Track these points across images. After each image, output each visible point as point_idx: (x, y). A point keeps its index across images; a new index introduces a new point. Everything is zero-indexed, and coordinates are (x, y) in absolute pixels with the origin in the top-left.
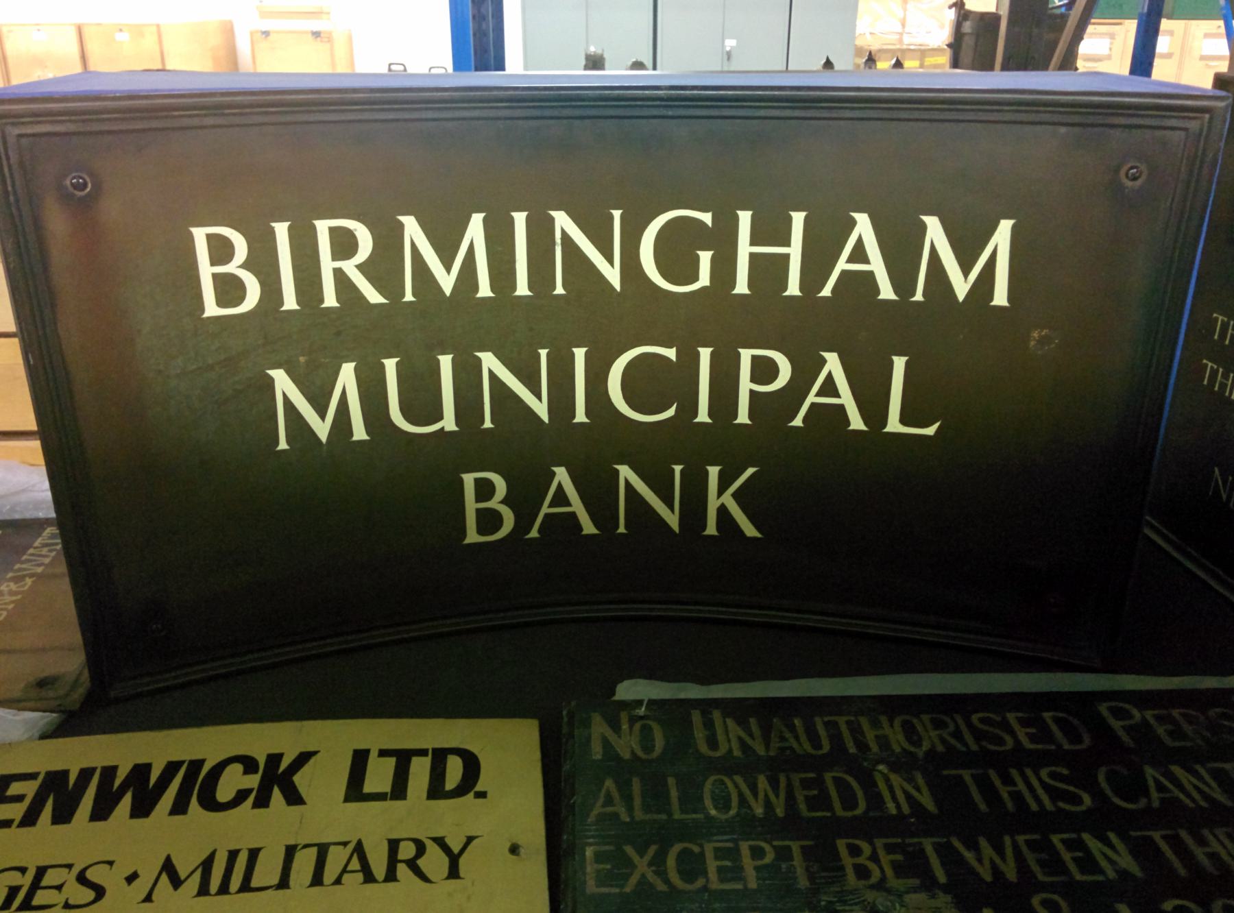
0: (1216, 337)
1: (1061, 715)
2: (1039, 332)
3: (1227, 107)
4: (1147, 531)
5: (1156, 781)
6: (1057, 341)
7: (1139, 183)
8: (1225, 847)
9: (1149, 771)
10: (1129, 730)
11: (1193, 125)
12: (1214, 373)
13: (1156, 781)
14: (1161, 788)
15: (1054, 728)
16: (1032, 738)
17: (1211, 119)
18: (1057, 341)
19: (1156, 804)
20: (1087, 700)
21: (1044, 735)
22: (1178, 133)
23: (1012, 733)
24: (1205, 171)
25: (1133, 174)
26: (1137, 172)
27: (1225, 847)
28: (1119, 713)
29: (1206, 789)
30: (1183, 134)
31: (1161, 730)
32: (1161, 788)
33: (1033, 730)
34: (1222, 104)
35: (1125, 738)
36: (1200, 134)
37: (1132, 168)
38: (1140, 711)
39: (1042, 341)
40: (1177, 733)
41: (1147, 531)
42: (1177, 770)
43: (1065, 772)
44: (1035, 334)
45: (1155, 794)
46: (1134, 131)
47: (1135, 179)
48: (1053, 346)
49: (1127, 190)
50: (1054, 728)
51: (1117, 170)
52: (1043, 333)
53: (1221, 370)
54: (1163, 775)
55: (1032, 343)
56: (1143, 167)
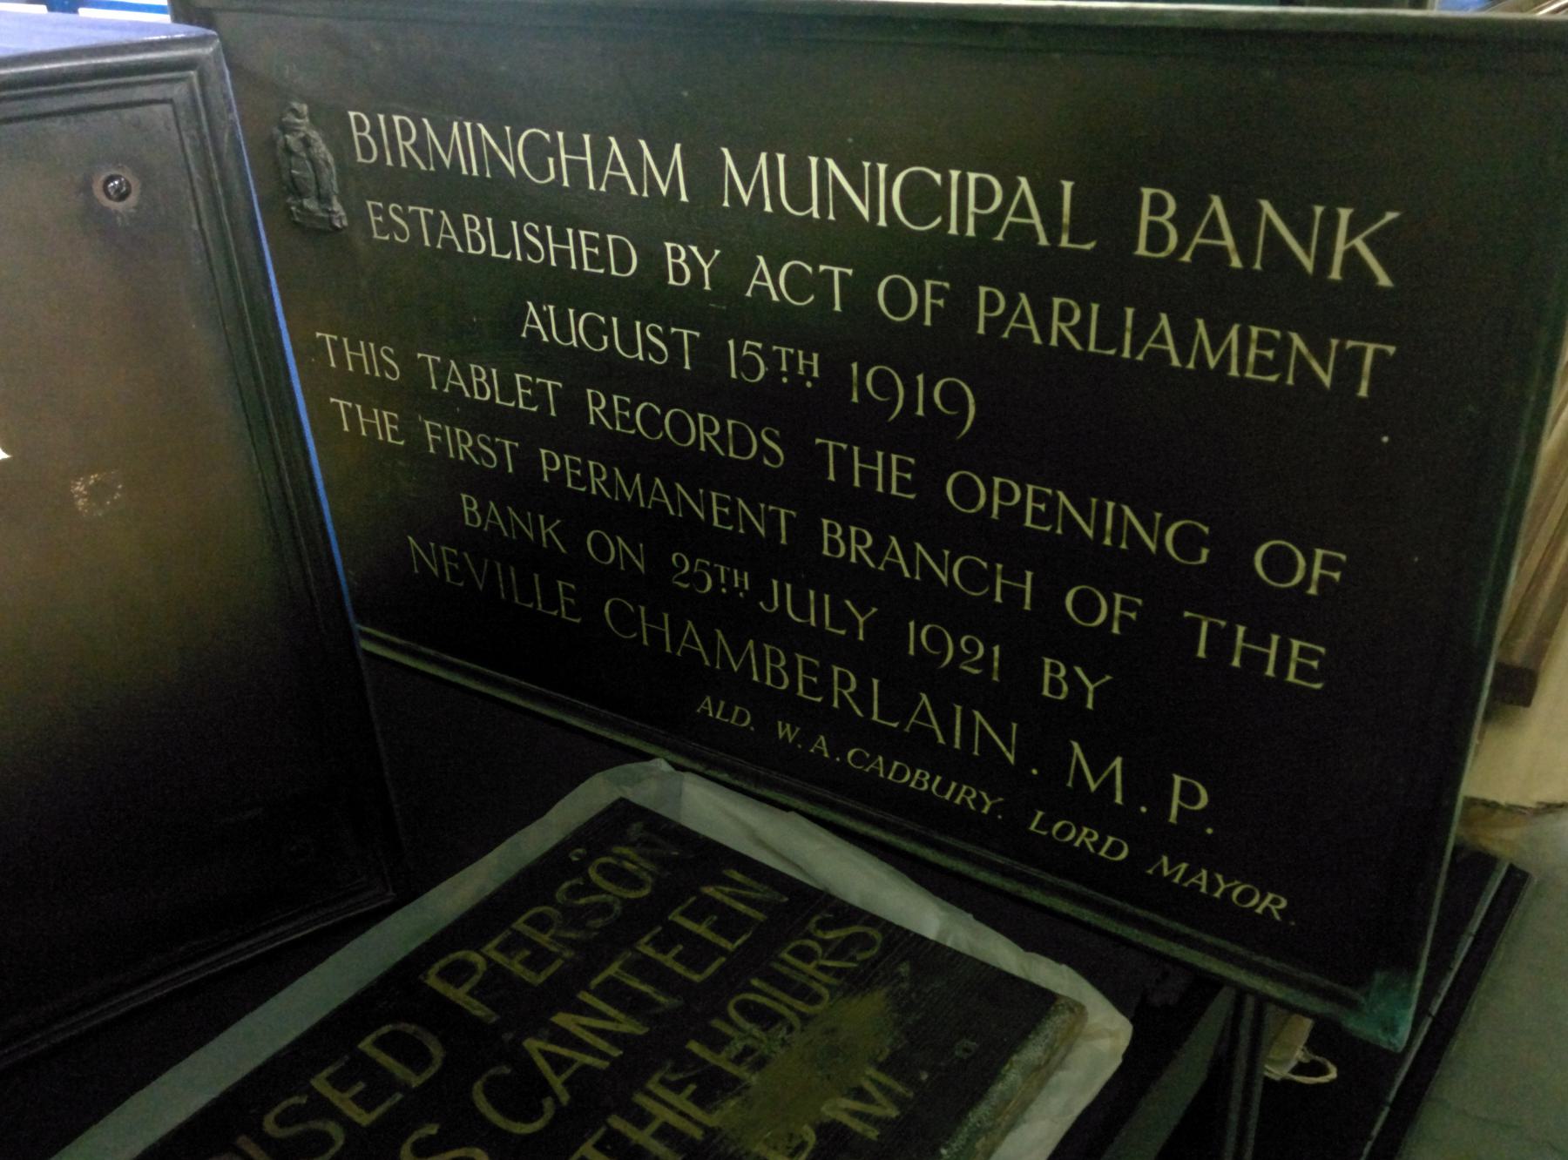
0: (333, 365)
1: (385, 1029)
2: (83, 482)
3: (215, 53)
4: (365, 645)
5: (547, 1056)
6: (120, 487)
7: (132, 199)
8: (671, 1107)
9: (533, 1045)
10: (478, 993)
11: (178, 92)
12: (351, 414)
13: (547, 1056)
14: (558, 1064)
15: (385, 1060)
16: (366, 1102)
17: (201, 77)
18: (120, 487)
19: (565, 1098)
20: (405, 974)
21: (377, 1086)
22: (157, 108)
23: (333, 1113)
24: (231, 163)
25: (118, 190)
26: (121, 184)
27: (671, 1107)
28: (456, 974)
29: (608, 1026)
30: (167, 108)
31: (517, 968)
32: (558, 1064)
33: (360, 1087)
34: (208, 51)
35: (479, 1010)
36: (194, 101)
37: (111, 179)
38: (477, 950)
39: (95, 493)
40: (539, 958)
41: (365, 645)
42: (562, 1019)
43: (432, 1130)
44: (79, 488)
45: (557, 1082)
46: (83, 116)
47: (122, 197)
48: (117, 496)
49: (119, 219)
50: (385, 1060)
51: (86, 188)
52: (92, 482)
53: (359, 407)
54: (552, 1041)
55: (81, 503)
56: (127, 175)
